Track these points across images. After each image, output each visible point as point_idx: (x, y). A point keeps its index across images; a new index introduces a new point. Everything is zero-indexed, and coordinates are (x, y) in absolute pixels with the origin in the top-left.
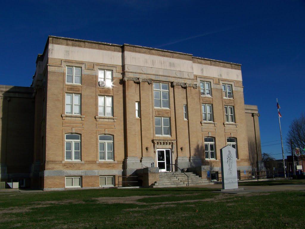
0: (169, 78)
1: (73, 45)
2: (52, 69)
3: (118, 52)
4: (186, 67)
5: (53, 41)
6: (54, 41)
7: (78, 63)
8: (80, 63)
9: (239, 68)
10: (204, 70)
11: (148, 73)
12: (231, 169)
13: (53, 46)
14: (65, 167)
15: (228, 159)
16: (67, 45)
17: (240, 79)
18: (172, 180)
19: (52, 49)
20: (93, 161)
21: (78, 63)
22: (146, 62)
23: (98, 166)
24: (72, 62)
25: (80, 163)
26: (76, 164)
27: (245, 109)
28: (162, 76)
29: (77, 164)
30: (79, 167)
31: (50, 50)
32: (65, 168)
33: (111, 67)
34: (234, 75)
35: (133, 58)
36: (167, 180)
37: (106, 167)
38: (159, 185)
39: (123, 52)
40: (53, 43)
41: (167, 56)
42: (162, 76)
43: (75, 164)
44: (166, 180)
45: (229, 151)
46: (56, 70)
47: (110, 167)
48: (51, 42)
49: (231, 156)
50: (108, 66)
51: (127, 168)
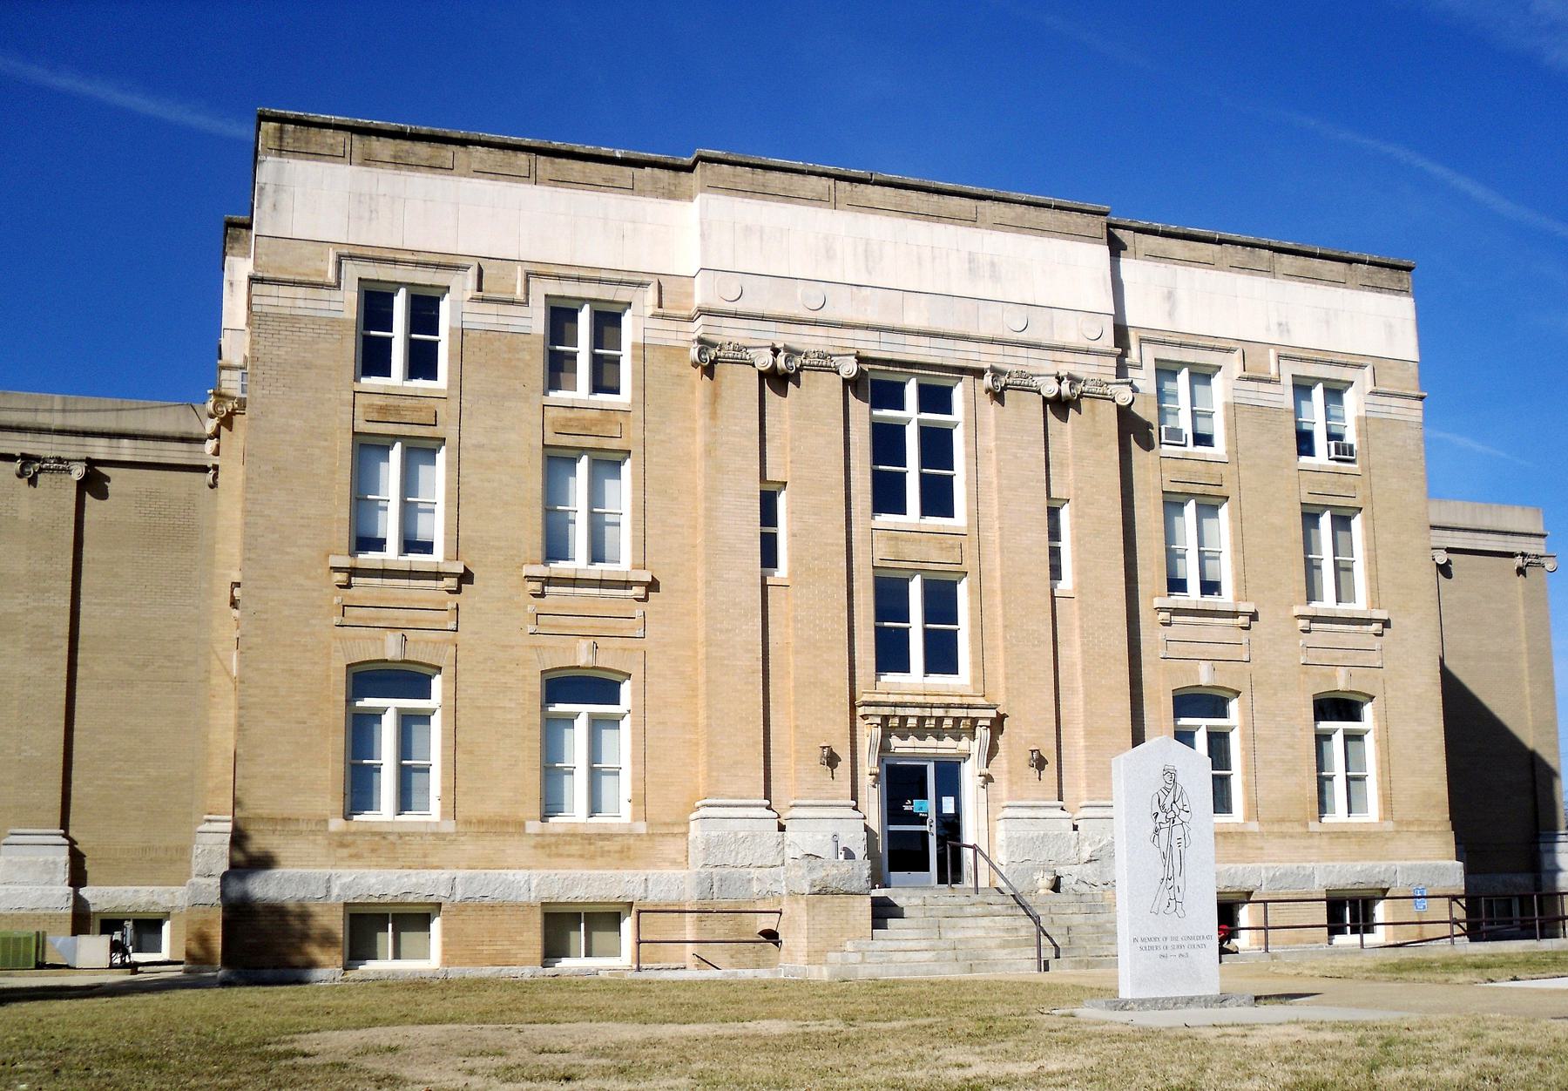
0: (961, 345)
1: (398, 163)
2: (274, 301)
3: (663, 196)
4: (1001, 281)
5: (281, 139)
6: (288, 140)
7: (426, 265)
8: (438, 266)
9: (1400, 281)
10: (1182, 294)
11: (1058, 340)
12: (1179, 881)
13: (279, 171)
14: (345, 852)
15: (1161, 818)
16: (368, 161)
17: (1407, 347)
18: (951, 935)
19: (278, 188)
20: (506, 823)
21: (426, 265)
22: (830, 254)
23: (535, 847)
24: (395, 262)
25: (433, 834)
26: (407, 834)
27: (1433, 527)
28: (919, 333)
29: (413, 834)
30: (425, 856)
31: (262, 189)
32: (342, 859)
33: (620, 283)
34: (1374, 324)
35: (748, 229)
36: (922, 934)
37: (582, 856)
38: (863, 962)
39: (1116, 248)
40: (280, 151)
41: (953, 219)
42: (919, 333)
43: (400, 836)
44: (911, 934)
45: (1170, 774)
46: (300, 303)
47: (604, 853)
48: (271, 144)
49: (1179, 804)
50: (600, 281)
51: (91, 901)
